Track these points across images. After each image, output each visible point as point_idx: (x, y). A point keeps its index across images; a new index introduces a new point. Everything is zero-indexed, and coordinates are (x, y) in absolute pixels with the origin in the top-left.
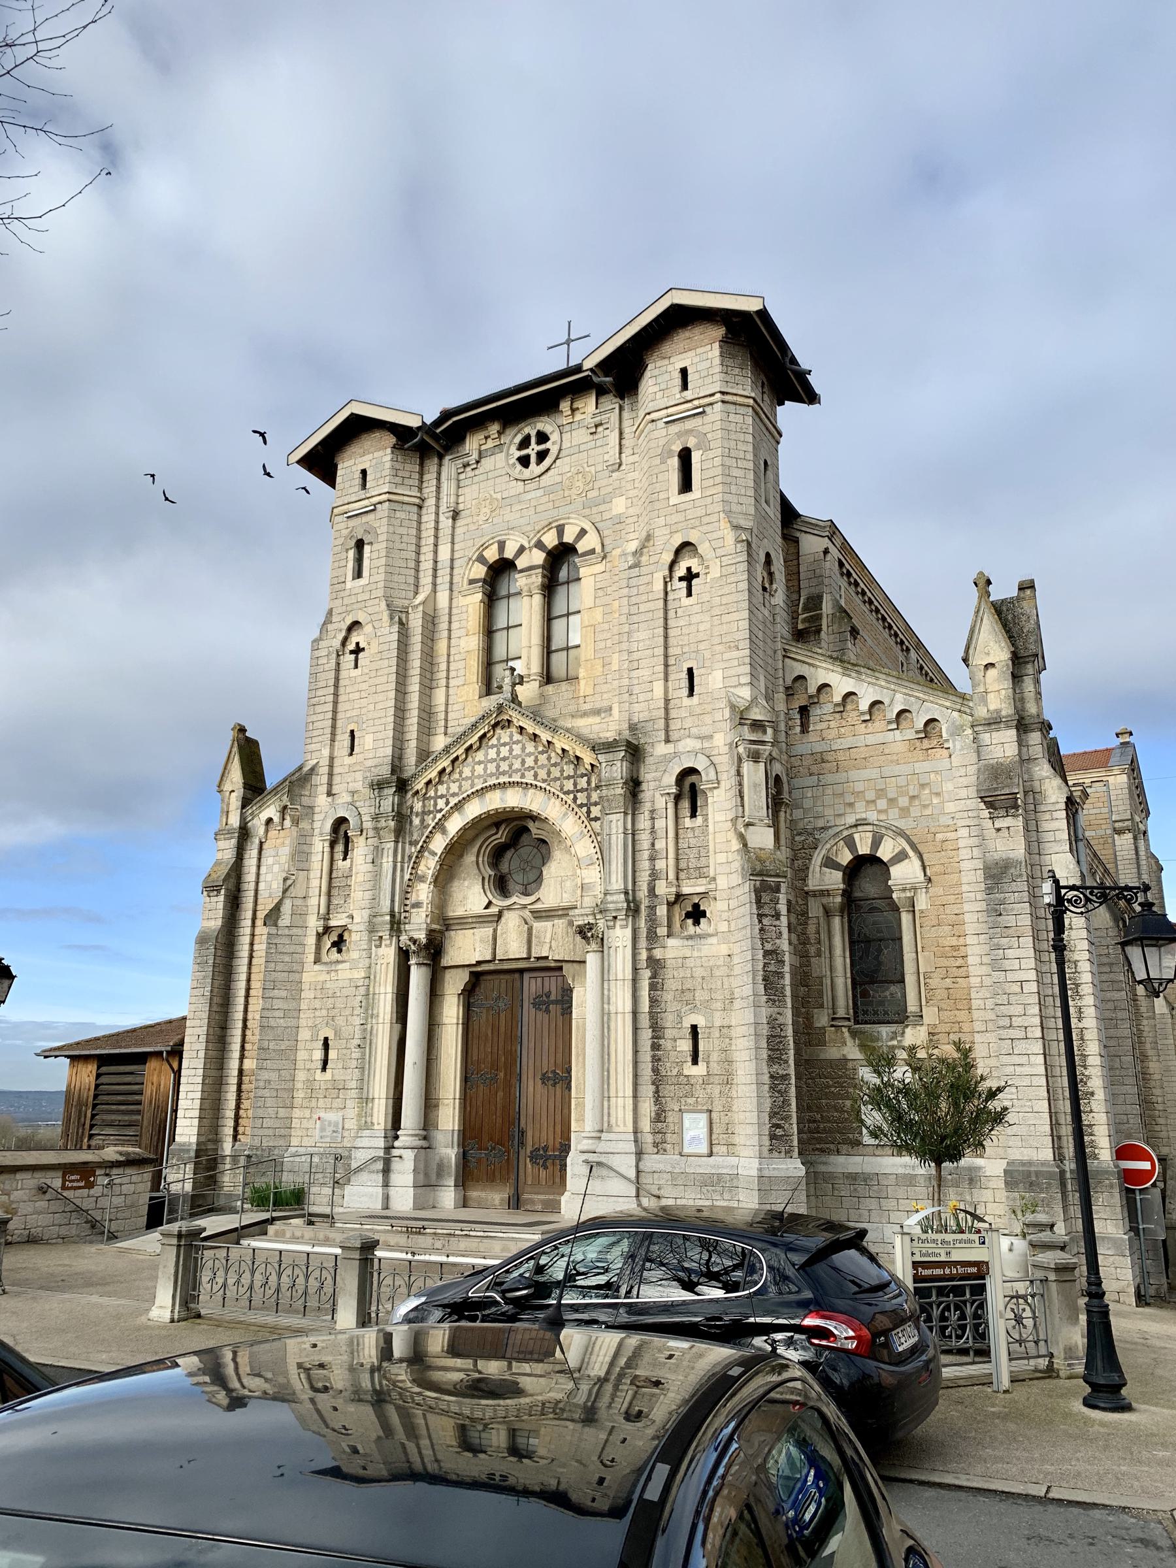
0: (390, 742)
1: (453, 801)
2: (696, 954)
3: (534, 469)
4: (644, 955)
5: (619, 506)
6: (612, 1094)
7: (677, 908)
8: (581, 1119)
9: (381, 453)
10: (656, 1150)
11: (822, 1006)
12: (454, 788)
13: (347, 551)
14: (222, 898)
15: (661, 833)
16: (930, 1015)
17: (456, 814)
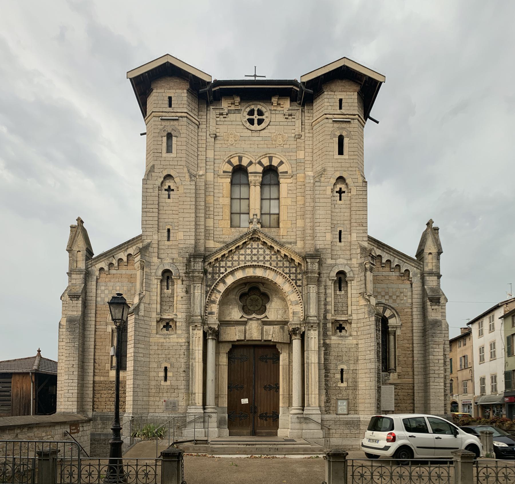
1: (229, 270)
2: (343, 343)
3: (256, 127)
4: (322, 342)
9: (180, 91)
12: (229, 264)
13: (162, 137)
14: (80, 302)
15: (328, 295)
16: (399, 369)
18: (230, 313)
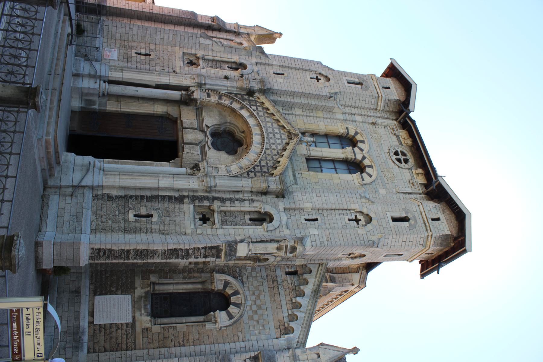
0: (280, 88)
1: (255, 113)
2: (186, 218)
4: (185, 194)
5: (382, 191)
6: (121, 177)
7: (207, 210)
8: (109, 163)
9: (397, 95)
10: (94, 195)
11: (160, 278)
12: (261, 114)
14: (210, 22)
16: (156, 329)
17: (249, 114)
18: (211, 117)
